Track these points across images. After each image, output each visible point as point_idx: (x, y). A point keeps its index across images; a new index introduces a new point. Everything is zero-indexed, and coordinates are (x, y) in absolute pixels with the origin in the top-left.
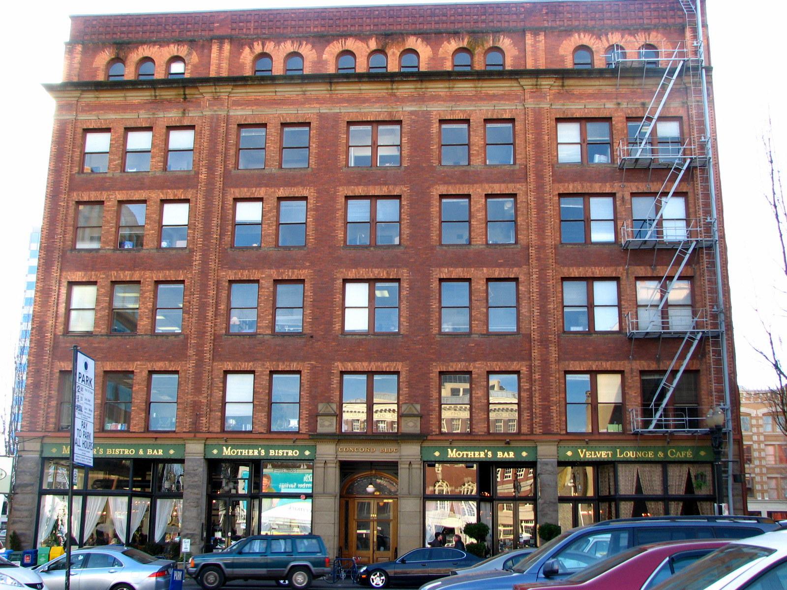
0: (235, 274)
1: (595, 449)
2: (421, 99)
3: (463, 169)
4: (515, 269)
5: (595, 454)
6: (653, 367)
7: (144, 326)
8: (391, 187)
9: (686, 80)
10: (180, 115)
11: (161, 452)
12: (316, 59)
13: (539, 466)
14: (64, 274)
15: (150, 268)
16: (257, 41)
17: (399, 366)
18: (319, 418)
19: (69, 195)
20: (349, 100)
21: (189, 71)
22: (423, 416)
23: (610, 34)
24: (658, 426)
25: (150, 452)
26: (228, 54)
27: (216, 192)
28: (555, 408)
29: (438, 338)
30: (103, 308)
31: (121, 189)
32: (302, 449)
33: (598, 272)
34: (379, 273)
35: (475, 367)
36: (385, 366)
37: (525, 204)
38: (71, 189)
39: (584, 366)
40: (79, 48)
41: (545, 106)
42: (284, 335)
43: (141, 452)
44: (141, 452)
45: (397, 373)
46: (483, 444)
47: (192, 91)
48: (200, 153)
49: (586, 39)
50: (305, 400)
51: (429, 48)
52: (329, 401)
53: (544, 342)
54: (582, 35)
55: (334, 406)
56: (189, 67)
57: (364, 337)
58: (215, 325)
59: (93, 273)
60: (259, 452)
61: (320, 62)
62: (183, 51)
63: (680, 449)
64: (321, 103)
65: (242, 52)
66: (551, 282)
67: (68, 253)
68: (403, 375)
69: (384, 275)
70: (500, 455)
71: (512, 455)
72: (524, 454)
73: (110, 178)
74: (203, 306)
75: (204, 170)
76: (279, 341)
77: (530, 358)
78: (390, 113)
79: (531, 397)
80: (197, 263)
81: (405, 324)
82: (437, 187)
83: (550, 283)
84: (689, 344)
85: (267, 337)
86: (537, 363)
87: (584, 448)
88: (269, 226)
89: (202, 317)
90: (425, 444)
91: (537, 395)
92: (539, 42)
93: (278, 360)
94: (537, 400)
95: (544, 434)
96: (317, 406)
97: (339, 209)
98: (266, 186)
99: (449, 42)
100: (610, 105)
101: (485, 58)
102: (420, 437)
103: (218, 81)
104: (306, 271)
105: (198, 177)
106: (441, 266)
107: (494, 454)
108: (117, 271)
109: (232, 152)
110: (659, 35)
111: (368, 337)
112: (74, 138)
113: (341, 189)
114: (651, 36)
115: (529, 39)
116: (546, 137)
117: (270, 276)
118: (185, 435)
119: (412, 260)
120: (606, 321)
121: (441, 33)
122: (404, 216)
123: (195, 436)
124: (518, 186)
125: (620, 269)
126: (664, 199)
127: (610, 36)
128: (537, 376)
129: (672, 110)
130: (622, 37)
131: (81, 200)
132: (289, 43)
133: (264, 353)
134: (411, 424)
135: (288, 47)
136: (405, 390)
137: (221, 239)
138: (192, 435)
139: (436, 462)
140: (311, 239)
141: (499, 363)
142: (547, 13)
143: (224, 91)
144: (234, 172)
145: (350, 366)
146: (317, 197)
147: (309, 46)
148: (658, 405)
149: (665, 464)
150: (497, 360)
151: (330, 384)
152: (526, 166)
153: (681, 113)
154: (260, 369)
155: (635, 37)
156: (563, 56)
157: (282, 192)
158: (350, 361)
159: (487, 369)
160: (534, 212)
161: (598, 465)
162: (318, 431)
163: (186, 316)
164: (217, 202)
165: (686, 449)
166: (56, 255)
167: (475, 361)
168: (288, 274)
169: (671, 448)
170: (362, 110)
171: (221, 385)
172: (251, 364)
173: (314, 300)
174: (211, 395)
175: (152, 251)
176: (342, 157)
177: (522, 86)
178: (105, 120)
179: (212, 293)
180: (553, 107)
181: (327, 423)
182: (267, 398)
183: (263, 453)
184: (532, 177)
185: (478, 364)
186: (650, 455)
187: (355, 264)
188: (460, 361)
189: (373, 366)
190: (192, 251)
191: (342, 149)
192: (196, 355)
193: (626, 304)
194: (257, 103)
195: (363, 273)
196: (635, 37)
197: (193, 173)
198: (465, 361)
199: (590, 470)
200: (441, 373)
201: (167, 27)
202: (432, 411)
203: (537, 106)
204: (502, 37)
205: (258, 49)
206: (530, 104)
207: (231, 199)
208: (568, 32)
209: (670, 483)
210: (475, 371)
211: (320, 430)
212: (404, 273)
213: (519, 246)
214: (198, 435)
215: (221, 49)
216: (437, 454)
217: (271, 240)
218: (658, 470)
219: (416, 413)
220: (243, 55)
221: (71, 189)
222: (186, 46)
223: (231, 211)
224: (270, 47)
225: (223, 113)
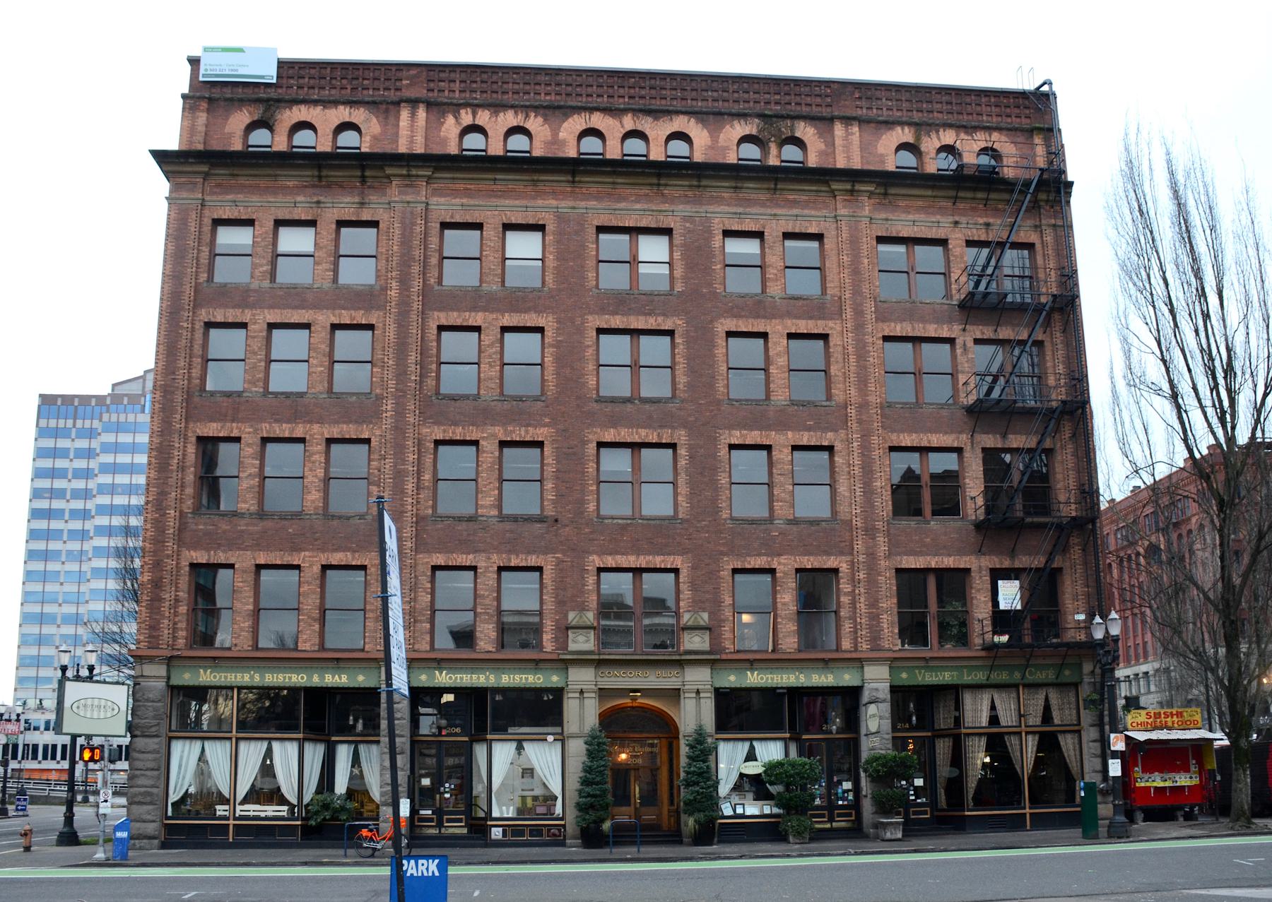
0: (444, 431)
7: (313, 501)
8: (660, 319)
14: (191, 425)
15: (320, 421)
18: (570, 632)
31: (271, 307)
34: (647, 436)
35: (779, 564)
36: (658, 561)
37: (840, 349)
61: (555, 141)
65: (443, 123)
76: (508, 526)
80: (389, 414)
81: (684, 504)
82: (722, 320)
91: (862, 600)
92: (853, 134)
93: (510, 552)
94: (862, 606)
96: (566, 616)
98: (485, 310)
106: (731, 427)
109: (434, 261)
113: (590, 318)
116: (866, 261)
117: (494, 435)
119: (692, 419)
124: (831, 323)
127: (941, 132)
131: (213, 320)
134: (697, 639)
137: (421, 382)
141: (812, 558)
145: (610, 561)
146: (558, 329)
150: (810, 554)
154: (484, 564)
158: (610, 554)
160: (852, 359)
164: (414, 330)
165: (1047, 666)
166: (179, 397)
167: (780, 555)
171: (429, 585)
172: (471, 556)
173: (558, 471)
174: (415, 600)
177: (833, 191)
179: (411, 457)
184: (849, 313)
185: (783, 559)
188: (759, 555)
189: (642, 562)
190: (380, 398)
202: (724, 621)
205: (467, 118)
207: (435, 327)
210: (779, 568)
212: (681, 437)
215: (413, 115)
217: (493, 386)
219: (702, 623)
221: (196, 305)
223: (435, 344)
224: (483, 118)
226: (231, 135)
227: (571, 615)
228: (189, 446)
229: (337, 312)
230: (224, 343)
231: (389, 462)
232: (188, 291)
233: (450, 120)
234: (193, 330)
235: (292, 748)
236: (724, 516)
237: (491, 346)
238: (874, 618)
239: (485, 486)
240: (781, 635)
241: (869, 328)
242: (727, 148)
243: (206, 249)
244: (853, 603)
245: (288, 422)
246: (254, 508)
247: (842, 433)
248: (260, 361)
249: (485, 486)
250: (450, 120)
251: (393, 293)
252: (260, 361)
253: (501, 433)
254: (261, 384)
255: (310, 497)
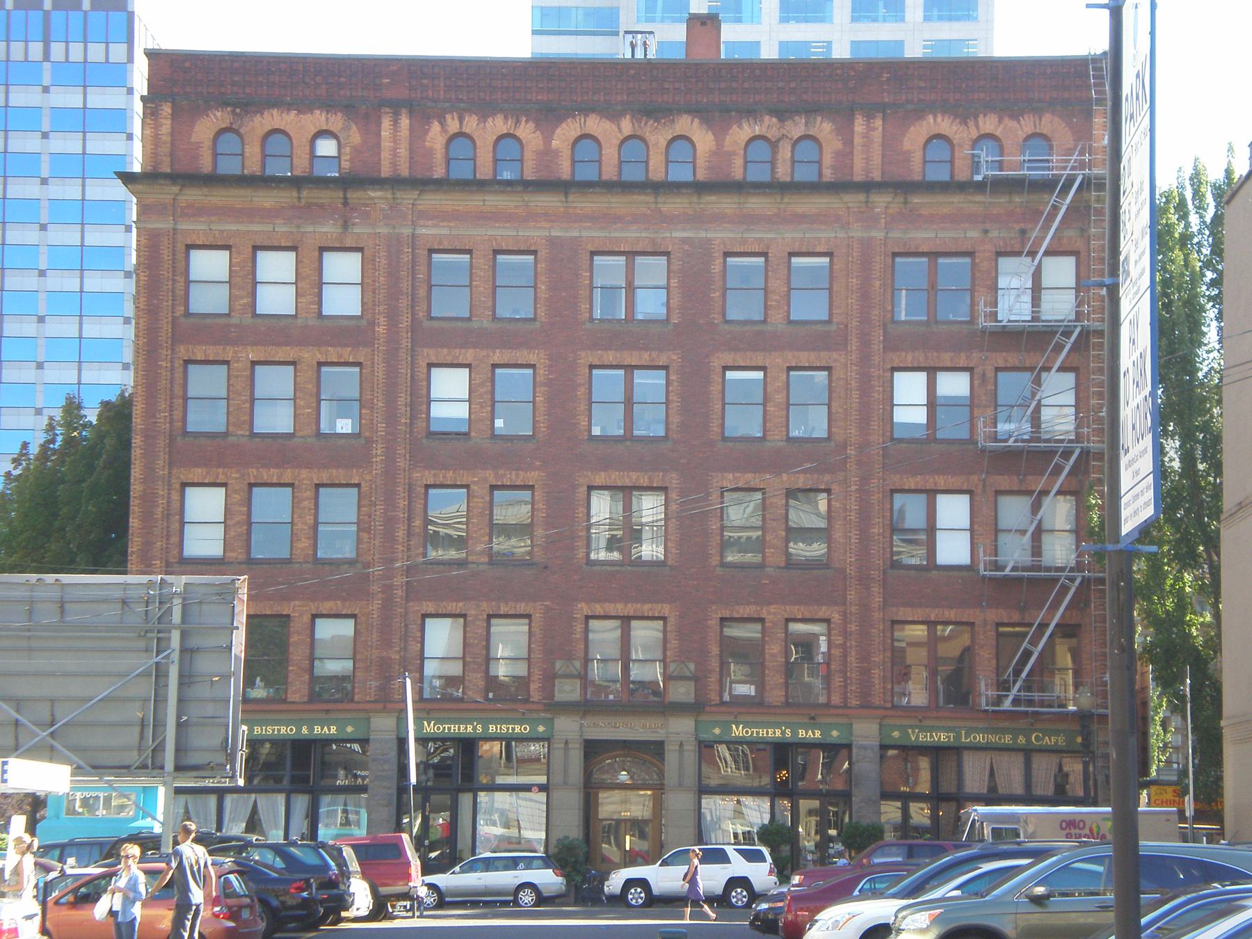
0: (435, 475)
1: (931, 729)
2: (698, 220)
3: (757, 328)
4: (827, 477)
5: (931, 736)
6: (1016, 617)
7: (302, 549)
8: (654, 354)
9: (1085, 195)
10: (340, 231)
11: (333, 730)
12: (542, 147)
13: (854, 750)
14: (175, 471)
15: (309, 466)
16: (451, 112)
17: (665, 609)
18: (557, 681)
19: (173, 350)
20: (592, 218)
21: (348, 157)
22: (698, 680)
23: (981, 116)
24: (1016, 701)
25: (317, 730)
26: (407, 133)
27: (402, 354)
28: (877, 671)
29: (719, 571)
30: (238, 522)
31: (255, 344)
32: (534, 723)
33: (941, 481)
34: (638, 479)
35: (769, 613)
36: (646, 609)
37: (842, 383)
38: (176, 339)
39: (919, 614)
40: (167, 109)
41: (878, 234)
42: (900, 441)
43: (305, 730)
44: (305, 730)
45: (664, 619)
46: (778, 719)
47: (359, 194)
48: (374, 292)
49: (945, 125)
50: (537, 655)
51: (710, 136)
52: (569, 657)
53: (864, 580)
54: (939, 119)
55: (578, 664)
56: (348, 150)
57: (618, 568)
58: (409, 550)
59: (220, 470)
60: (475, 728)
61: (547, 154)
62: (336, 121)
63: (1049, 733)
64: (552, 221)
65: (428, 131)
66: (876, 497)
67: (179, 439)
68: (672, 621)
69: (644, 481)
70: (802, 733)
71: (818, 734)
72: (835, 733)
73: (236, 326)
74: (390, 522)
75: (382, 319)
77: (844, 603)
78: (653, 241)
79: (845, 655)
80: (379, 459)
81: (674, 551)
83: (875, 498)
84: (1065, 590)
85: (482, 567)
86: (854, 609)
87: (917, 727)
88: (482, 407)
89: (389, 537)
90: (703, 718)
91: (853, 653)
92: (874, 129)
94: (852, 659)
95: (861, 707)
96: (553, 664)
97: (580, 385)
99: (740, 126)
100: (974, 234)
101: (793, 152)
102: (695, 708)
103: (396, 182)
104: (535, 474)
105: (374, 331)
107: (795, 733)
108: (258, 469)
109: (422, 292)
110: (1056, 119)
111: (623, 569)
112: (173, 259)
113: (583, 354)
114: (1044, 119)
115: (859, 125)
116: (878, 283)
118: (368, 706)
119: (685, 461)
120: (953, 549)
121: (728, 111)
122: (673, 397)
123: (385, 707)
124: (835, 355)
125: (975, 478)
126: (1044, 375)
127: (981, 119)
128: (853, 627)
129: (1065, 241)
130: (1000, 121)
131: (193, 358)
132: (499, 119)
133: (476, 589)
134: (682, 690)
135: (498, 125)
136: (673, 643)
137: (411, 424)
138: (380, 706)
139: (716, 742)
140: (542, 427)
141: (802, 608)
142: (888, 79)
143: (407, 197)
144: (426, 324)
145: (598, 609)
146: (550, 366)
147: (531, 125)
148: (1017, 672)
149: (1028, 753)
151: (571, 633)
152: (846, 326)
153: (1079, 245)
155: (1019, 122)
156: (909, 152)
157: (497, 357)
159: (786, 616)
160: (855, 394)
161: (937, 752)
162: (556, 699)
163: (365, 535)
164: (404, 369)
165: (1057, 733)
166: (161, 442)
168: (510, 477)
169: (1036, 730)
170: (613, 235)
172: (461, 604)
174: (405, 648)
175: (309, 440)
176: (584, 306)
178: (222, 231)
179: (402, 503)
180: (890, 235)
181: (567, 688)
182: (484, 652)
183: (479, 728)
184: (854, 343)
185: (773, 608)
186: (1007, 739)
187: (606, 464)
188: (749, 603)
189: (630, 609)
190: (370, 441)
191: (584, 293)
192: (383, 592)
193: (984, 528)
194: (457, 216)
195: (616, 478)
196: (1019, 122)
197: (364, 322)
198: (755, 603)
199: (924, 764)
200: (722, 619)
201: (307, 80)
203: (865, 235)
204: (819, 119)
205: (453, 125)
206: (857, 232)
207: (424, 365)
208: (919, 114)
209: (1034, 779)
211: (559, 697)
213: (833, 444)
214: (389, 706)
215: (396, 122)
216: (717, 731)
218: (1019, 760)
219: (688, 674)
220: (431, 134)
221: (176, 339)
222: (339, 115)
223: (425, 383)
224: (471, 124)
225: (407, 231)
226: (198, 146)
227: (558, 664)
228: (173, 492)
229: (323, 349)
230: (207, 382)
231: (380, 507)
232: (166, 328)
233: (436, 127)
234: (172, 369)
235: (281, 799)
236: (714, 563)
237: (482, 384)
238: (865, 672)
239: (475, 532)
240: (767, 688)
241: (876, 359)
242: (733, 153)
243: (181, 279)
244: (845, 655)
245: (277, 466)
246: (242, 557)
247: (840, 476)
248: (245, 402)
249: (475, 532)
250: (436, 127)
251: (381, 330)
252: (245, 402)
253: (490, 476)
254: (247, 427)
255: (299, 545)
